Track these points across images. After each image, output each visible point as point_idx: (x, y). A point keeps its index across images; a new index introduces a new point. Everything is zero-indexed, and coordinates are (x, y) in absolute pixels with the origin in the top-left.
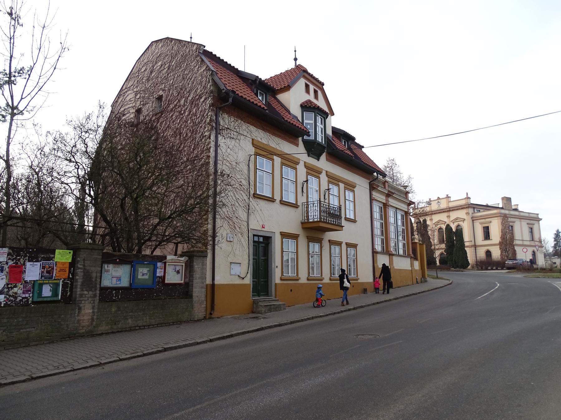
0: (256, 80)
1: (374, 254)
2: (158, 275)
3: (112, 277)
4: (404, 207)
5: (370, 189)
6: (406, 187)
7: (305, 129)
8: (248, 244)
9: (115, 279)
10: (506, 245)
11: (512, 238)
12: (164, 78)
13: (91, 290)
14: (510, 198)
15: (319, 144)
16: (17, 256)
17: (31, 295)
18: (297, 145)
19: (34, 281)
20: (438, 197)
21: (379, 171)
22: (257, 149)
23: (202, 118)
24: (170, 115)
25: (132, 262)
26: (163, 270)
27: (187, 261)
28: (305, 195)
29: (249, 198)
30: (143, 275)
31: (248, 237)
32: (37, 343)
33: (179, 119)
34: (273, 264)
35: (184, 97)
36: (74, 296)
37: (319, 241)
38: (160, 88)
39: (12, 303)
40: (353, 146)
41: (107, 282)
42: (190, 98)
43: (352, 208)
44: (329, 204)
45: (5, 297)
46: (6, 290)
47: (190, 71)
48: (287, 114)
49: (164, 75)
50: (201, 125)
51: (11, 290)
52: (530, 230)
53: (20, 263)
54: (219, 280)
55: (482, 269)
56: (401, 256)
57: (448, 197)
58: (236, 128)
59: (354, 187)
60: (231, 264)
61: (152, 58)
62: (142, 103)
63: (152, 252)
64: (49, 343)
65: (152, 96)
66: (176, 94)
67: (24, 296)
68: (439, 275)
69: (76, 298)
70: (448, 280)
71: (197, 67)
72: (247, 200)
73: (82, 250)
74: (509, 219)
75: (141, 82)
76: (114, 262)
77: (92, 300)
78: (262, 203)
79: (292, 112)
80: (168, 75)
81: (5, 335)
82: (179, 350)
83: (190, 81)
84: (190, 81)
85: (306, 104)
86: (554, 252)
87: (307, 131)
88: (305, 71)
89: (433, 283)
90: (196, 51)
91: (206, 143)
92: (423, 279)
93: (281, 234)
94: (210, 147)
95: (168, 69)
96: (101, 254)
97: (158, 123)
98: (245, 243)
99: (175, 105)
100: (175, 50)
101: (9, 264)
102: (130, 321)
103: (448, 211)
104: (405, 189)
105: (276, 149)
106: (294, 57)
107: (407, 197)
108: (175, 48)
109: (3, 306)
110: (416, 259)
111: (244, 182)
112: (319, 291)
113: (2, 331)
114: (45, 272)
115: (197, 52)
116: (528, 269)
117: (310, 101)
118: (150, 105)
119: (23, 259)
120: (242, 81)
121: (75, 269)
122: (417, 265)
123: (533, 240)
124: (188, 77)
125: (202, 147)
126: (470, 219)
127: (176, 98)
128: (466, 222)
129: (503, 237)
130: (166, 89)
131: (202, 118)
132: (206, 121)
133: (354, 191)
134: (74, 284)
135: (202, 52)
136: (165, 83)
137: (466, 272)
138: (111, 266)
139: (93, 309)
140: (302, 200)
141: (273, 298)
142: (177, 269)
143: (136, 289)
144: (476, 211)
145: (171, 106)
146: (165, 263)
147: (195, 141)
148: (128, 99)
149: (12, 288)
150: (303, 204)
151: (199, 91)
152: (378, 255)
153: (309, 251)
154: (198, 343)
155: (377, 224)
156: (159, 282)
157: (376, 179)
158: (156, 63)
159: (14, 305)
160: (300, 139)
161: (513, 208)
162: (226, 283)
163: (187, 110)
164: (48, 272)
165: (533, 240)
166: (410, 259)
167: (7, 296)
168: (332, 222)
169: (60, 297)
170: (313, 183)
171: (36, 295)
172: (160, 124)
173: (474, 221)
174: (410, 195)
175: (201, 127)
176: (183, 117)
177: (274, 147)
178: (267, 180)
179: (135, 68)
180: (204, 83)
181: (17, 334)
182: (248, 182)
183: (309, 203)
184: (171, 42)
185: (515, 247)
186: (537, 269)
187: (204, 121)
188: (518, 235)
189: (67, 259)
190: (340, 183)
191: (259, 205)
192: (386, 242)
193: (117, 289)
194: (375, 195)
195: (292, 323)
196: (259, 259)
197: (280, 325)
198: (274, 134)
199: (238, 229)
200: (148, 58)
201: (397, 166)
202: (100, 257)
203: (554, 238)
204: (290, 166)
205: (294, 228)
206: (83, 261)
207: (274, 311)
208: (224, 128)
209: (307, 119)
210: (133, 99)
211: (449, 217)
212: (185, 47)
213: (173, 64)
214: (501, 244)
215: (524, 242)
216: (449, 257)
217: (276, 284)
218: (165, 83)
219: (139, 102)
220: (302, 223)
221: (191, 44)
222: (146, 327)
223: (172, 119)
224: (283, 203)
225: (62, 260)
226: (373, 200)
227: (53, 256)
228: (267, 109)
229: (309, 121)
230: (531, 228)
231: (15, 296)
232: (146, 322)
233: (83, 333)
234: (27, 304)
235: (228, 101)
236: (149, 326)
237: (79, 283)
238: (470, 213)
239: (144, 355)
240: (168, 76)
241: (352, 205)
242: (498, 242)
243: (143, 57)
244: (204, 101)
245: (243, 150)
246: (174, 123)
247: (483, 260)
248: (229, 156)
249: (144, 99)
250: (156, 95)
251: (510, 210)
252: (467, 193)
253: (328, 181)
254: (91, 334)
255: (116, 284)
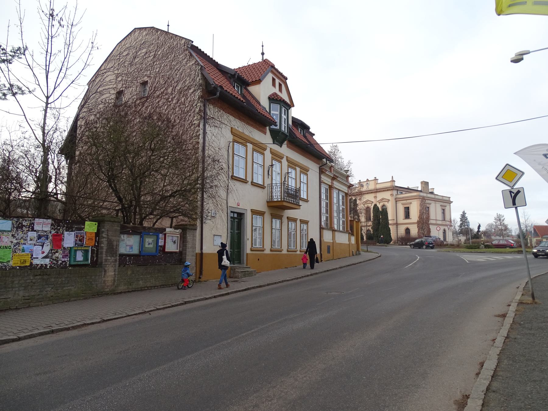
0: (235, 75)
1: (321, 230)
2: (160, 244)
3: (126, 246)
4: (345, 189)
5: (320, 173)
6: (347, 172)
7: (273, 120)
8: (227, 219)
9: (128, 247)
10: (423, 224)
11: (428, 218)
12: (149, 65)
13: (113, 256)
14: (428, 183)
15: (283, 133)
16: (58, 226)
17: (68, 259)
18: (265, 133)
19: (70, 247)
20: (367, 179)
21: (328, 158)
22: (235, 137)
23: (190, 108)
24: (157, 101)
25: (141, 233)
26: (163, 241)
27: (181, 233)
28: (270, 177)
29: (228, 180)
30: (149, 244)
31: (227, 213)
32: (75, 299)
33: (166, 106)
34: (245, 237)
35: (171, 86)
36: (99, 260)
37: (280, 217)
38: (145, 74)
39: (55, 265)
40: (307, 135)
41: (123, 250)
42: (178, 88)
43: (305, 190)
44: (288, 185)
45: (50, 261)
46: (50, 255)
47: (177, 63)
48: (258, 105)
49: (150, 63)
50: (190, 114)
51: (54, 255)
52: (442, 211)
53: (60, 232)
54: (205, 250)
55: (402, 245)
56: (341, 232)
57: (376, 179)
58: (219, 117)
59: (308, 171)
60: (214, 237)
61: (135, 44)
62: (124, 86)
63: (154, 225)
64: (84, 299)
65: (135, 80)
66: (163, 82)
67: (63, 260)
68: (369, 250)
69: (102, 263)
70: (377, 253)
71: (186, 60)
72: (227, 182)
73: (106, 222)
74: (426, 201)
75: (123, 65)
76: (128, 233)
77: (114, 265)
78: (238, 184)
79: (262, 104)
80: (154, 63)
81: (53, 292)
82: (193, 304)
83: (177, 72)
84: (177, 72)
85: (273, 97)
86: (460, 230)
87: (275, 122)
88: (273, 66)
89: (365, 256)
90: (185, 46)
91: (195, 130)
92: (357, 252)
93: (252, 212)
94: (199, 134)
95: (154, 57)
96: (120, 226)
97: (143, 107)
98: (225, 219)
99: (162, 93)
100: (161, 40)
101: (52, 233)
102: (141, 282)
103: (375, 192)
104: (346, 173)
105: (243, 133)
106: (261, 52)
107: (347, 180)
108: (162, 38)
109: (48, 268)
110: (353, 235)
111: (225, 166)
112: (186, 270)
113: (51, 288)
114: (78, 240)
115: (186, 46)
116: (440, 245)
117: (276, 94)
118: (134, 89)
119: (62, 229)
120: (222, 74)
121: (100, 238)
122: (353, 239)
123: (444, 219)
124: (175, 68)
125: (191, 134)
126: (394, 200)
127: (163, 86)
128: (390, 202)
129: (421, 217)
130: (152, 76)
131: (190, 108)
132: (194, 111)
133: (307, 175)
134: (99, 250)
135: (190, 47)
136: (150, 70)
137: (389, 247)
138: (125, 236)
139: (115, 271)
140: (268, 182)
141: (245, 265)
142: (174, 240)
143: (143, 256)
144: (399, 193)
145: (158, 93)
146: (165, 235)
147: (184, 127)
148: (108, 79)
149: (55, 253)
150: (269, 185)
151: (187, 82)
152: (324, 230)
153: (272, 226)
154: (206, 299)
155: (324, 204)
156: (160, 250)
157: (325, 164)
158: (140, 49)
159: (56, 267)
160: (268, 128)
161: (430, 191)
162: (210, 252)
163: (175, 99)
164: (80, 240)
165: (444, 220)
166: (348, 235)
167: (51, 260)
168: (291, 201)
169: (89, 262)
170: (277, 167)
171: (72, 259)
172: (146, 107)
173: (397, 202)
174: (350, 178)
175: (190, 115)
176: (171, 104)
177: (247, 134)
178: (242, 163)
179: (115, 51)
180: (192, 76)
181: (61, 291)
182: (227, 166)
183: (273, 185)
184: (157, 32)
185: (430, 225)
186: (448, 245)
187: (193, 110)
188: (432, 216)
189: (93, 230)
190: (297, 168)
191: (235, 186)
192: (330, 219)
193: (130, 256)
194: (324, 178)
195: (268, 285)
196: (234, 232)
197: (260, 287)
198: (248, 124)
199: (219, 206)
200: (131, 43)
201: (339, 151)
202: (119, 228)
203: (461, 219)
204: (261, 152)
205: (261, 206)
206: (107, 232)
207: (247, 276)
208: (210, 117)
209: (273, 110)
210: (114, 81)
211: (375, 197)
212: (173, 39)
213: (159, 53)
214: (418, 223)
215: (438, 221)
216: (375, 234)
217: (247, 254)
218: (150, 70)
219: (121, 85)
220: (267, 202)
221: (179, 37)
222: (152, 288)
223: (158, 105)
224: (253, 184)
225: (90, 230)
226: (322, 182)
227: (83, 227)
228: (245, 102)
229: (275, 112)
230: (444, 210)
231: (57, 260)
232: (153, 283)
233: (108, 291)
234: (65, 267)
235: (216, 95)
236: (154, 287)
237: (104, 250)
238: (394, 195)
239: (173, 306)
240: (154, 64)
241: (305, 186)
242: (416, 221)
243: (124, 41)
244: (193, 92)
245: (224, 137)
246: (161, 109)
247: (403, 237)
248: (214, 142)
249: (127, 82)
250: (141, 80)
251: (427, 193)
252: (392, 177)
253: (288, 165)
254: (114, 293)
255: (129, 252)
